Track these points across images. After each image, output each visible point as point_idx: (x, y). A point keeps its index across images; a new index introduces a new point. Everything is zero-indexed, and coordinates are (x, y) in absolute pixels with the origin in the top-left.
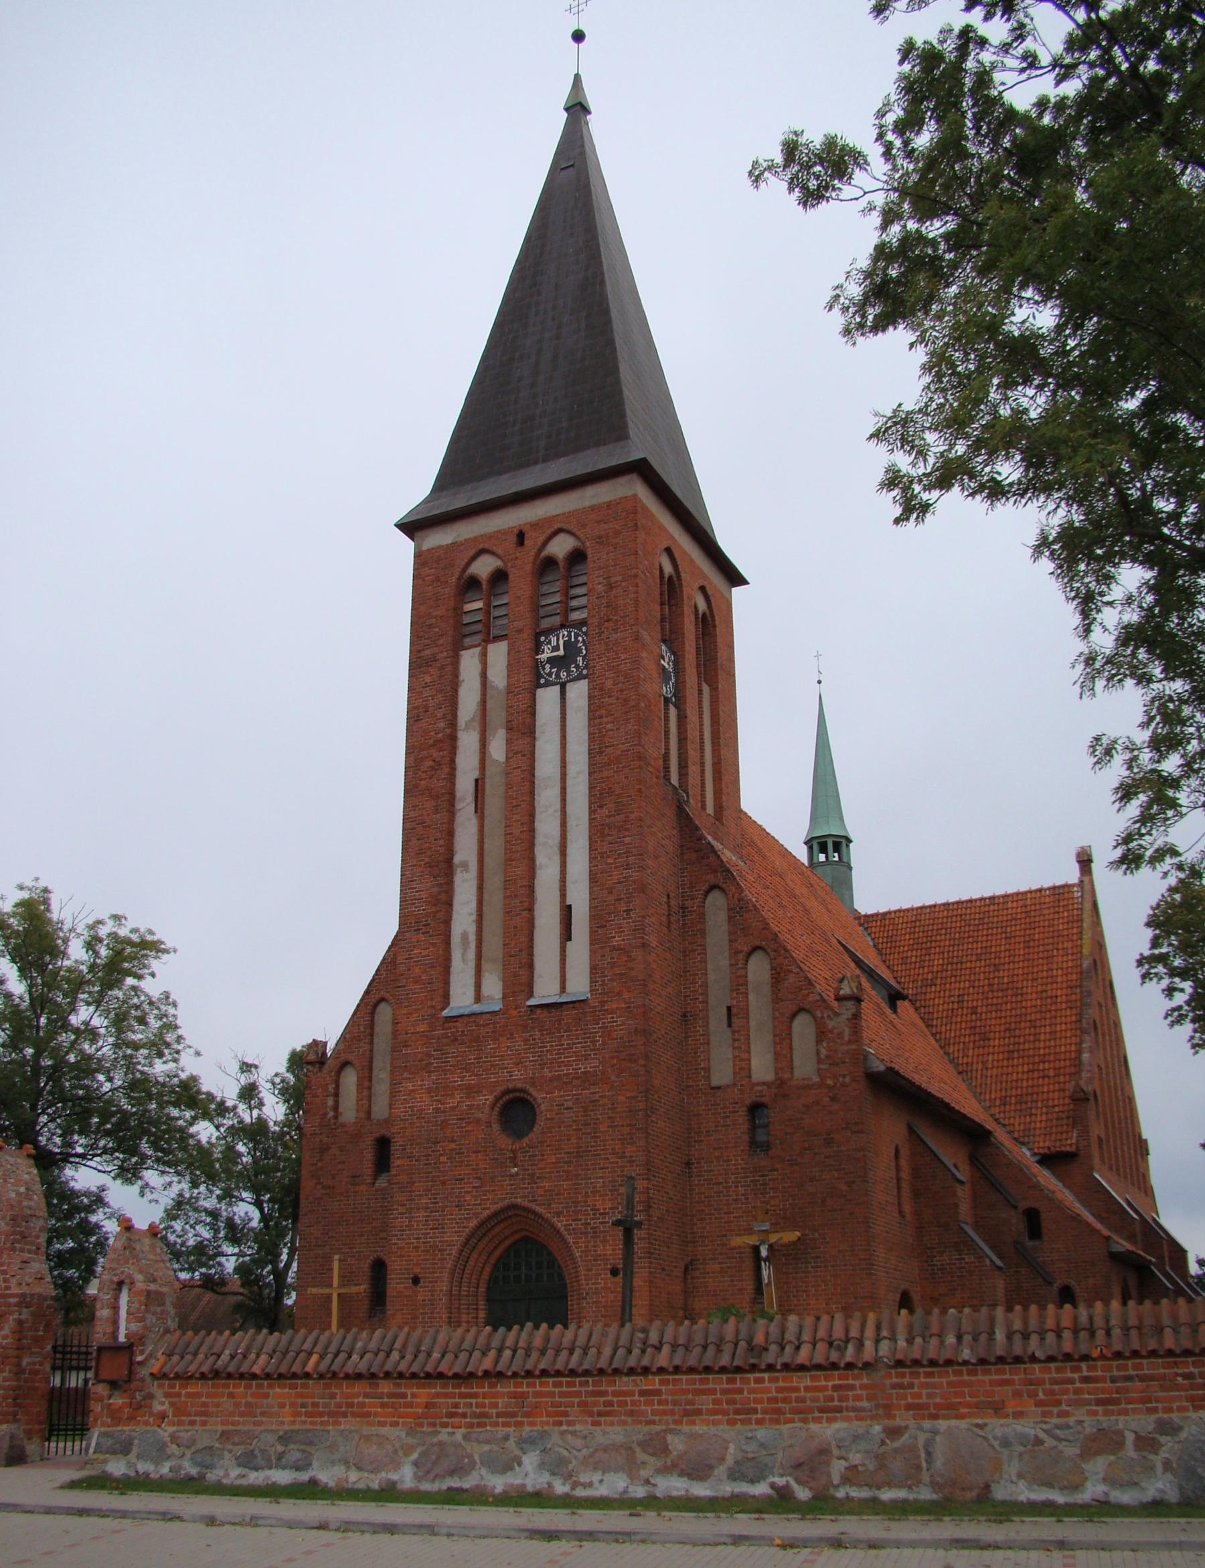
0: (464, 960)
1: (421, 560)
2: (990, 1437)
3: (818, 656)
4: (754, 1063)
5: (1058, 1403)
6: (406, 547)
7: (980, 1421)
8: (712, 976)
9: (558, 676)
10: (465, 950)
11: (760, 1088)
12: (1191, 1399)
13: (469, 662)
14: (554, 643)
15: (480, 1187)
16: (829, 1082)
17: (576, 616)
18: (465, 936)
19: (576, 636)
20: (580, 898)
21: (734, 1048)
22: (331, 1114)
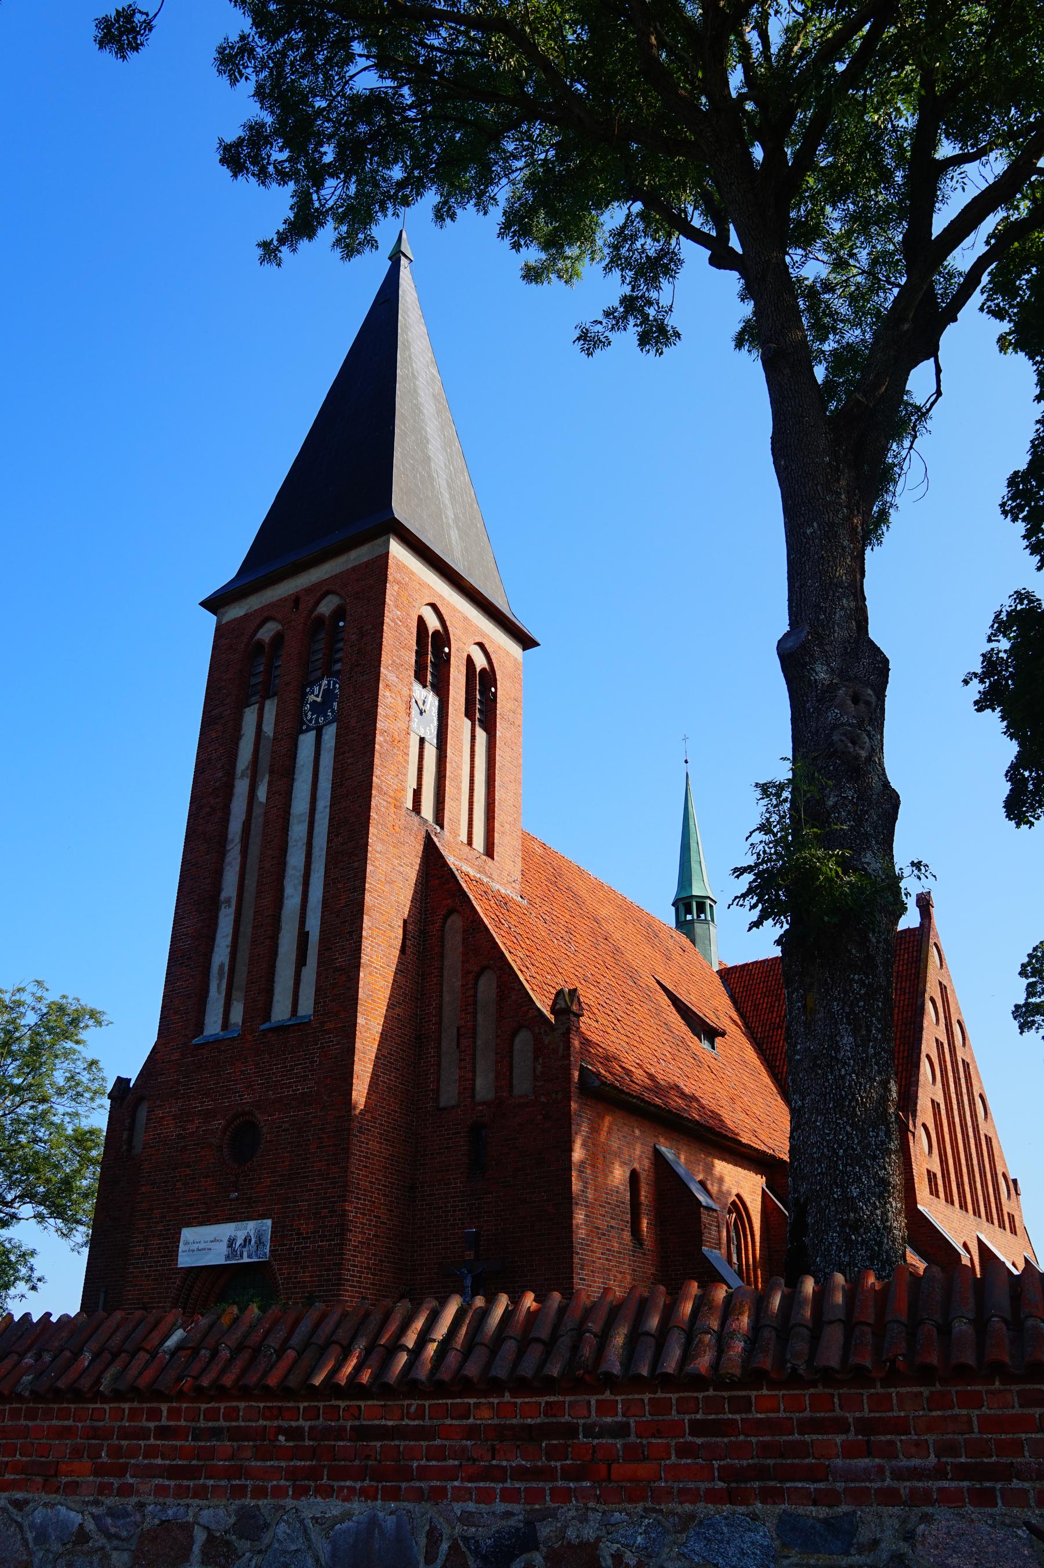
0: (219, 992)
1: (221, 632)
2: (26, 1524)
3: (685, 739)
4: (479, 1082)
5: (121, 1471)
6: (209, 621)
7: (19, 1496)
8: (446, 998)
9: (317, 721)
10: (221, 980)
11: (480, 1108)
12: (292, 1474)
13: (250, 716)
14: (316, 692)
15: (205, 1213)
16: (543, 1099)
17: (338, 667)
18: (221, 966)
19: (335, 683)
20: (314, 924)
21: (460, 1068)
22: (125, 1147)
